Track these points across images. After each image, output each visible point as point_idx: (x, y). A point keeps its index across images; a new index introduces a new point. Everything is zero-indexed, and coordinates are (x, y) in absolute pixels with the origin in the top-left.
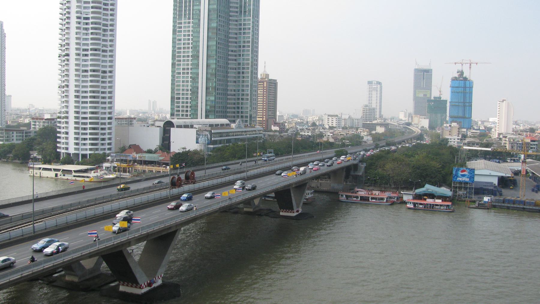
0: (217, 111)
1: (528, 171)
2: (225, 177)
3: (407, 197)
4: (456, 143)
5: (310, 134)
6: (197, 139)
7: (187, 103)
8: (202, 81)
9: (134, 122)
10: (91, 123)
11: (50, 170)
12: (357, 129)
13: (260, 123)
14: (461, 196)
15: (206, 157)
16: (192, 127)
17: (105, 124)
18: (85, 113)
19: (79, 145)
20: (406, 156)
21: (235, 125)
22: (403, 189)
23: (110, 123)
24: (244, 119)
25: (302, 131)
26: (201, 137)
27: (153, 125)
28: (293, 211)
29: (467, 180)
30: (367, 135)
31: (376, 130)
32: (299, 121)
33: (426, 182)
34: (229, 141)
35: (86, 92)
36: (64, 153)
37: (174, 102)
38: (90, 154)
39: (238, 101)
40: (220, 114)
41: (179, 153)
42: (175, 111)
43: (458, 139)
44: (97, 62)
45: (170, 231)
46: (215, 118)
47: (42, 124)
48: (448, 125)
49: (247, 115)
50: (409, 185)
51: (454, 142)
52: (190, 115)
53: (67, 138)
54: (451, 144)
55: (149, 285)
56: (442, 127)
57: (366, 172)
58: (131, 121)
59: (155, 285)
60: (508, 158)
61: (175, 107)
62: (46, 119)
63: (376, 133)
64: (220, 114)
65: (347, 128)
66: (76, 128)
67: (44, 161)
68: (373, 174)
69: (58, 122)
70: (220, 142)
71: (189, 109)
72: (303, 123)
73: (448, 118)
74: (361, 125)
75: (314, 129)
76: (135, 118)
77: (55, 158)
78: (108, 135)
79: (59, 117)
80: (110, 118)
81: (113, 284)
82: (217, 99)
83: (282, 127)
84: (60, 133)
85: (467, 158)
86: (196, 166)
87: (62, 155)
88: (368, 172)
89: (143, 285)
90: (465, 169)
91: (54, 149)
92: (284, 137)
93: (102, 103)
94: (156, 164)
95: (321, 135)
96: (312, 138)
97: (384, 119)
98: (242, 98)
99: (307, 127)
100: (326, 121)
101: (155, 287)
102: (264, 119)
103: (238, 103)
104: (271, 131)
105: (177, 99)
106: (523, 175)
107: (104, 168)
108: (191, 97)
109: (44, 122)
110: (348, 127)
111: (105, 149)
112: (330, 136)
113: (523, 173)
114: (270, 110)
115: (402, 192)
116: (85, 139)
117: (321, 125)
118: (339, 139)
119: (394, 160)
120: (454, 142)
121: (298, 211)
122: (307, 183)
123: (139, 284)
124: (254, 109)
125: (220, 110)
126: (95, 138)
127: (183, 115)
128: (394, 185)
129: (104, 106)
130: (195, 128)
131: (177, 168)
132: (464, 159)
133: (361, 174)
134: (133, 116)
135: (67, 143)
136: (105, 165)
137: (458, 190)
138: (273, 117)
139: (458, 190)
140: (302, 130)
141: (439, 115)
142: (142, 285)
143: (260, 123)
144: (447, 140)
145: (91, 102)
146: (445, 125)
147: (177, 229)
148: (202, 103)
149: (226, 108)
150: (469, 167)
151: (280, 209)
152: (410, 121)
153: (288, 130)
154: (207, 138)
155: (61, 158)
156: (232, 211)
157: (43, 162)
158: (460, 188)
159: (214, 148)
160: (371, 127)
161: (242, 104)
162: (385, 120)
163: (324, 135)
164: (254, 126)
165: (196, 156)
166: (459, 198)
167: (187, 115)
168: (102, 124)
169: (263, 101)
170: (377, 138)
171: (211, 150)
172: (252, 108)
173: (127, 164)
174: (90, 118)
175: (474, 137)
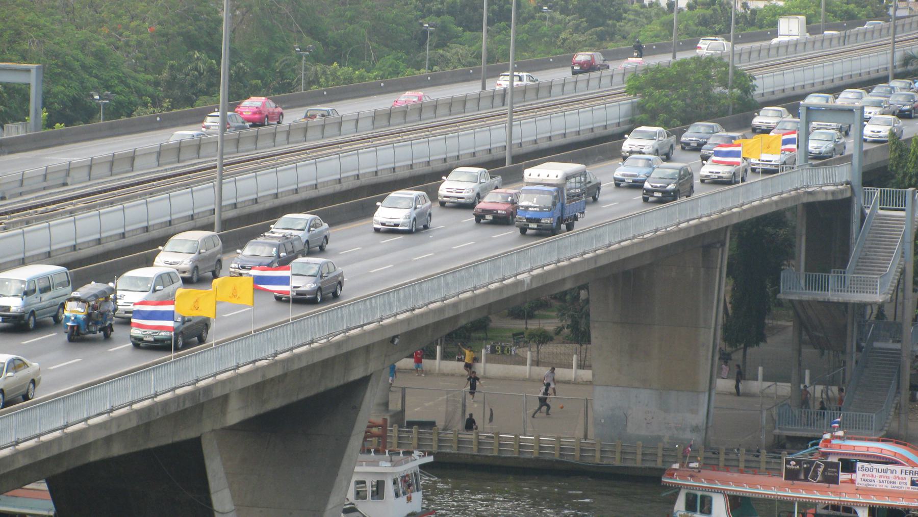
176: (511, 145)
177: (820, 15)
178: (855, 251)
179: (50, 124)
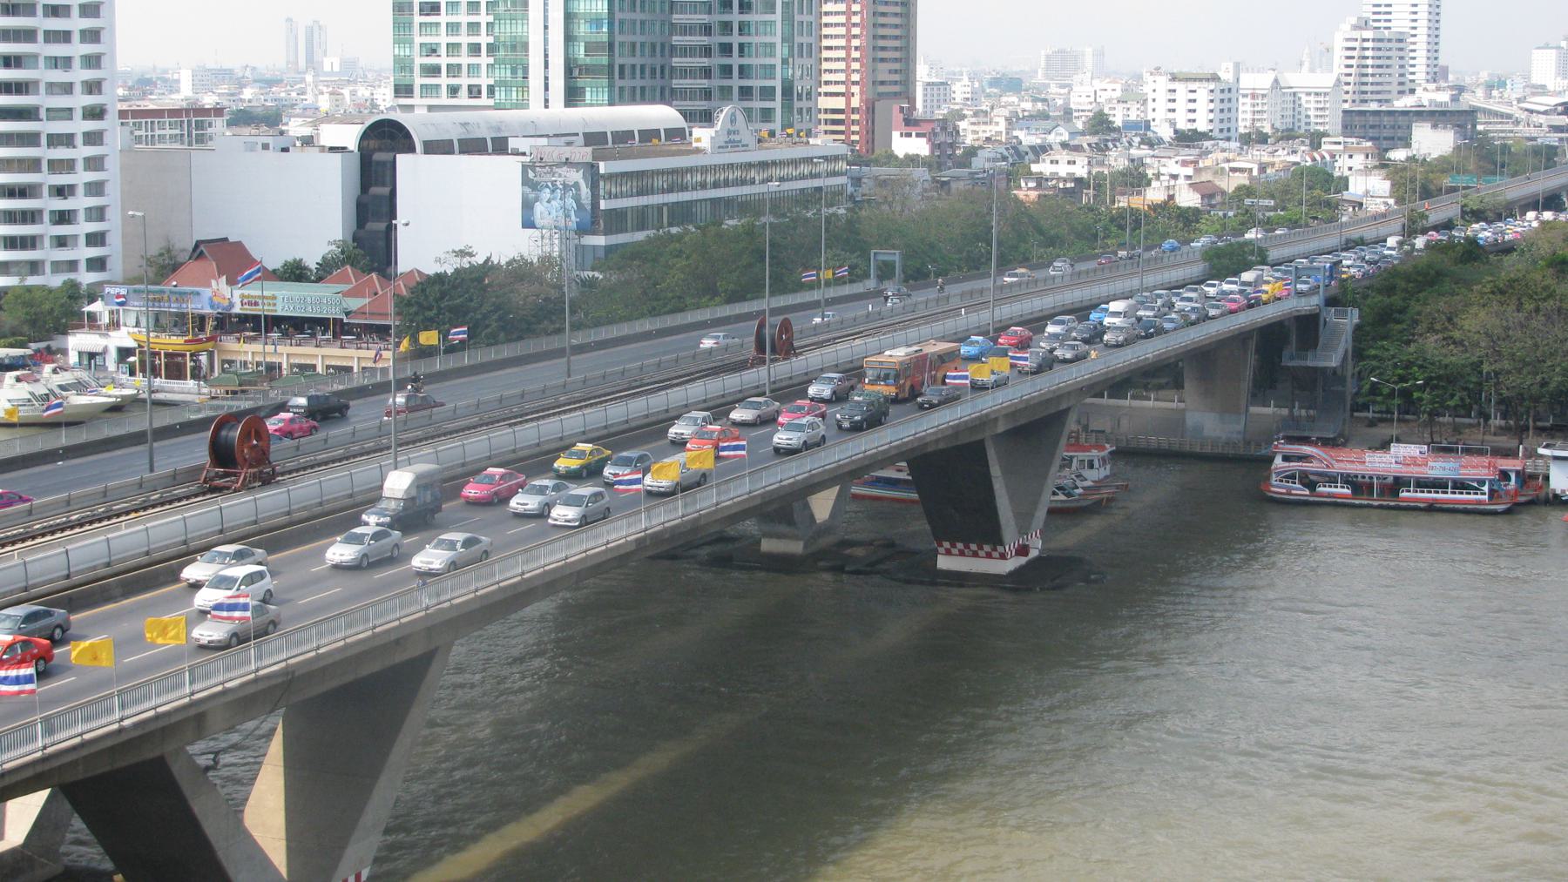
0: (622, 67)
5: (1080, 170)
6: (528, 206)
9: (218, 126)
12: (1316, 140)
13: (834, 122)
15: (570, 293)
16: (500, 147)
23: (93, 138)
24: (757, 104)
26: (546, 194)
28: (1000, 549)
30: (1367, 171)
31: (1408, 145)
40: (638, 83)
41: (440, 278)
42: (417, 70)
58: (200, 125)
63: (1412, 159)
68: (1395, 366)
70: (642, 218)
76: (218, 111)
80: (95, 113)
88: (1373, 352)
100: (1162, 105)
107: (73, 358)
111: (72, 265)
117: (1130, 126)
121: (1023, 550)
122: (1068, 409)
125: (638, 61)
127: (454, 91)
129: (59, 50)
140: (1040, 151)
143: (834, 122)
154: (577, 199)
159: (609, 249)
163: (1150, 172)
165: (524, 289)
172: (791, 49)
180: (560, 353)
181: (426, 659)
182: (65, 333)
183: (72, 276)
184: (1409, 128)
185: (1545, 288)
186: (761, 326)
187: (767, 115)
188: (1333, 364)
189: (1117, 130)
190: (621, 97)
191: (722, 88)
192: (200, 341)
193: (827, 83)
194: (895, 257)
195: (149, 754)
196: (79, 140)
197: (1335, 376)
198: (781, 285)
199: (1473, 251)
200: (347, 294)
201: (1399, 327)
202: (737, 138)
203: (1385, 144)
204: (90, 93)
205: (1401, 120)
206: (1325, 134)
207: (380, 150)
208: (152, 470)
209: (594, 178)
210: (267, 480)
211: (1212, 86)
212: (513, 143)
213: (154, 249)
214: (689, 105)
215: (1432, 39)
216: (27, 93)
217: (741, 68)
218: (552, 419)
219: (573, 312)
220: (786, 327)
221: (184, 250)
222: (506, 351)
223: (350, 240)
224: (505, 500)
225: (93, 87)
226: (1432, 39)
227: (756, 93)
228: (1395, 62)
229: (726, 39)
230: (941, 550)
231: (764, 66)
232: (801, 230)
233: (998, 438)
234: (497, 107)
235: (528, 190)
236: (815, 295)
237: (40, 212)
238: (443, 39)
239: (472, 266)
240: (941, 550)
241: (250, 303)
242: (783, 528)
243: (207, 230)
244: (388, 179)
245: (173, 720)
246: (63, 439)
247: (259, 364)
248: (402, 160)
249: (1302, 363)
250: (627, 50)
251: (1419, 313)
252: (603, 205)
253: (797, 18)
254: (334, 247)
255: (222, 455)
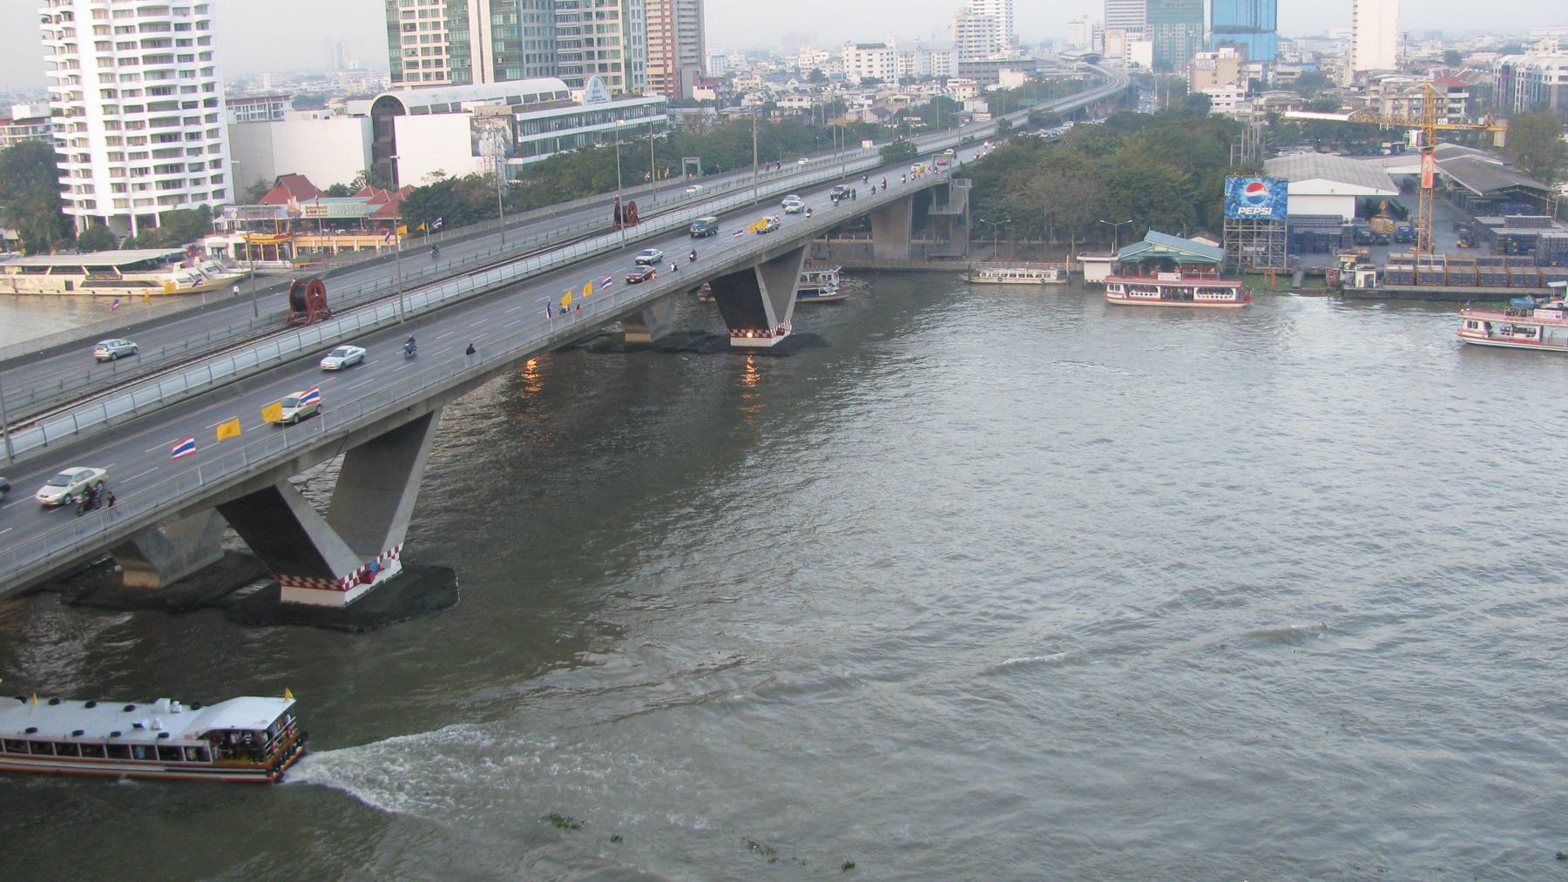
0: (527, 56)
1: (1441, 177)
2: (562, 247)
3: (1096, 271)
4: (1233, 105)
5: (806, 104)
6: (475, 143)
7: (437, 38)
8: (479, 7)
9: (287, 106)
10: (154, 122)
11: (41, 270)
12: (943, 80)
13: (658, 83)
14: (1251, 261)
15: (502, 193)
16: (457, 109)
17: (195, 120)
18: (132, 93)
19: (125, 191)
20: (1086, 153)
21: (584, 92)
22: (1083, 248)
23: (211, 118)
24: (610, 74)
25: (783, 97)
26: (485, 135)
27: (340, 112)
28: (767, 331)
29: (1267, 212)
30: (974, 98)
31: (997, 82)
32: (773, 67)
33: (1150, 224)
34: (568, 141)
35: (128, 29)
36: (84, 217)
37: (399, 39)
38: (162, 215)
39: (588, 23)
40: (538, 65)
41: (425, 189)
42: (404, 65)
43: (1239, 95)
44: (155, 14)
45: (411, 418)
46: (522, 78)
47: (7, 137)
48: (1209, 55)
49: (616, 61)
50: (1098, 238)
51: (1228, 104)
52: (447, 49)
53: (87, 173)
54: (1218, 111)
55: (365, 577)
56: (1192, 62)
57: (973, 205)
58: (275, 106)
59: (381, 577)
60: (1384, 145)
61: (403, 53)
62: (17, 122)
63: (1000, 90)
64: (538, 65)
65: (912, 81)
66: (111, 140)
67: (26, 247)
68: (994, 212)
69: (56, 126)
70: (545, 146)
71: (444, 57)
72: (783, 72)
73: (1207, 35)
74: (954, 70)
75: (818, 92)
76: (286, 97)
77: (59, 235)
78: (201, 59)
79: (58, 113)
80: (210, 103)
81: (257, 587)
82: (525, 21)
83: (722, 89)
84: (64, 158)
85: (1267, 148)
86: (475, 223)
87: (78, 223)
88: (981, 204)
89: (347, 579)
90: (1259, 181)
91: (54, 208)
92: (731, 117)
93: (182, 58)
94: (359, 226)
95: (838, 107)
96: (813, 118)
97: (1021, 48)
98: (597, 14)
99: (797, 85)
100: (853, 63)
101: (381, 582)
102: (670, 70)
103: (589, 29)
104: (692, 103)
105: (405, 30)
106: (1427, 190)
107: (209, 252)
108: (446, 19)
109: (13, 131)
110: (915, 76)
111: (204, 196)
112: (866, 108)
113: (1427, 183)
114: (684, 41)
115: (1078, 258)
116: (143, 171)
117: (836, 77)
118: (889, 113)
119: (1054, 165)
120: (1228, 104)
121: (780, 332)
122: (803, 247)
123: (335, 578)
124: (635, 43)
125: (537, 51)
126: (172, 166)
127: (427, 76)
128: (1057, 239)
129: (187, 66)
130: (467, 111)
131: (421, 234)
132: (1258, 151)
133: (959, 212)
134: (280, 91)
135: (90, 188)
136: (210, 241)
137: (1240, 243)
138: (694, 60)
139: (1240, 243)
140: (782, 94)
141: (1181, 28)
142: (343, 580)
143: (658, 83)
144: (1204, 101)
145: (148, 59)
146: (1199, 56)
147: (430, 410)
148: (480, 35)
149: (553, 19)
150: (1271, 175)
151: (731, 326)
152: (1098, 49)
153: (741, 96)
154: (504, 137)
155: (78, 234)
156: (590, 344)
157: (24, 250)
158: (1248, 237)
159: (525, 166)
160: (981, 72)
161: (599, 31)
162: (1025, 49)
163: (847, 104)
164: (639, 91)
165: (477, 192)
166: (1246, 266)
167: (440, 76)
168: (188, 121)
169: (663, 17)
170: (1001, 103)
171: (517, 172)
172: (629, 40)
173: (274, 233)
174: (152, 107)
175: (1286, 87)
176: (403, 313)
177: (1418, 837)
178: (950, 199)
179: (704, 175)
180: (498, 230)
181: (425, 421)
182: (202, 237)
183: (205, 202)
184: (997, 71)
185: (1079, 163)
186: (617, 208)
187: (616, 80)
188: (958, 212)
189: (827, 79)
190: (528, 74)
191: (588, 65)
192: (283, 237)
193: (652, 59)
194: (697, 161)
195: (267, 484)
196: (203, 120)
197: (959, 220)
198: (629, 183)
199: (1038, 143)
200: (369, 203)
201: (996, 189)
202: (598, 95)
203: (985, 82)
204: (208, 91)
205: (993, 67)
206: (950, 77)
207: (384, 114)
208: (257, 315)
209: (514, 125)
210: (327, 317)
211: (880, 51)
212: (464, 106)
213: (252, 183)
214: (569, 77)
215: (1009, 20)
216: (170, 93)
217: (599, 52)
218: (480, 275)
219: (504, 205)
220: (633, 206)
221: (270, 182)
222: (467, 231)
223: (369, 170)
224: (317, 361)
225: (209, 87)
226: (1009, 20)
227: (609, 68)
228: (988, 34)
229: (589, 36)
230: (732, 334)
231: (613, 51)
232: (640, 148)
233: (762, 266)
234: (454, 84)
235: (474, 133)
236: (650, 187)
237: (182, 164)
238: (419, 46)
239: (444, 181)
240: (732, 334)
241: (311, 212)
242: (637, 327)
243: (283, 169)
244: (390, 132)
245: (279, 463)
246: (204, 300)
247: (319, 248)
248: (398, 120)
249: (941, 213)
250: (529, 45)
251: (1006, 181)
252: (520, 140)
253: (631, 8)
254: (360, 175)
255: (298, 305)
